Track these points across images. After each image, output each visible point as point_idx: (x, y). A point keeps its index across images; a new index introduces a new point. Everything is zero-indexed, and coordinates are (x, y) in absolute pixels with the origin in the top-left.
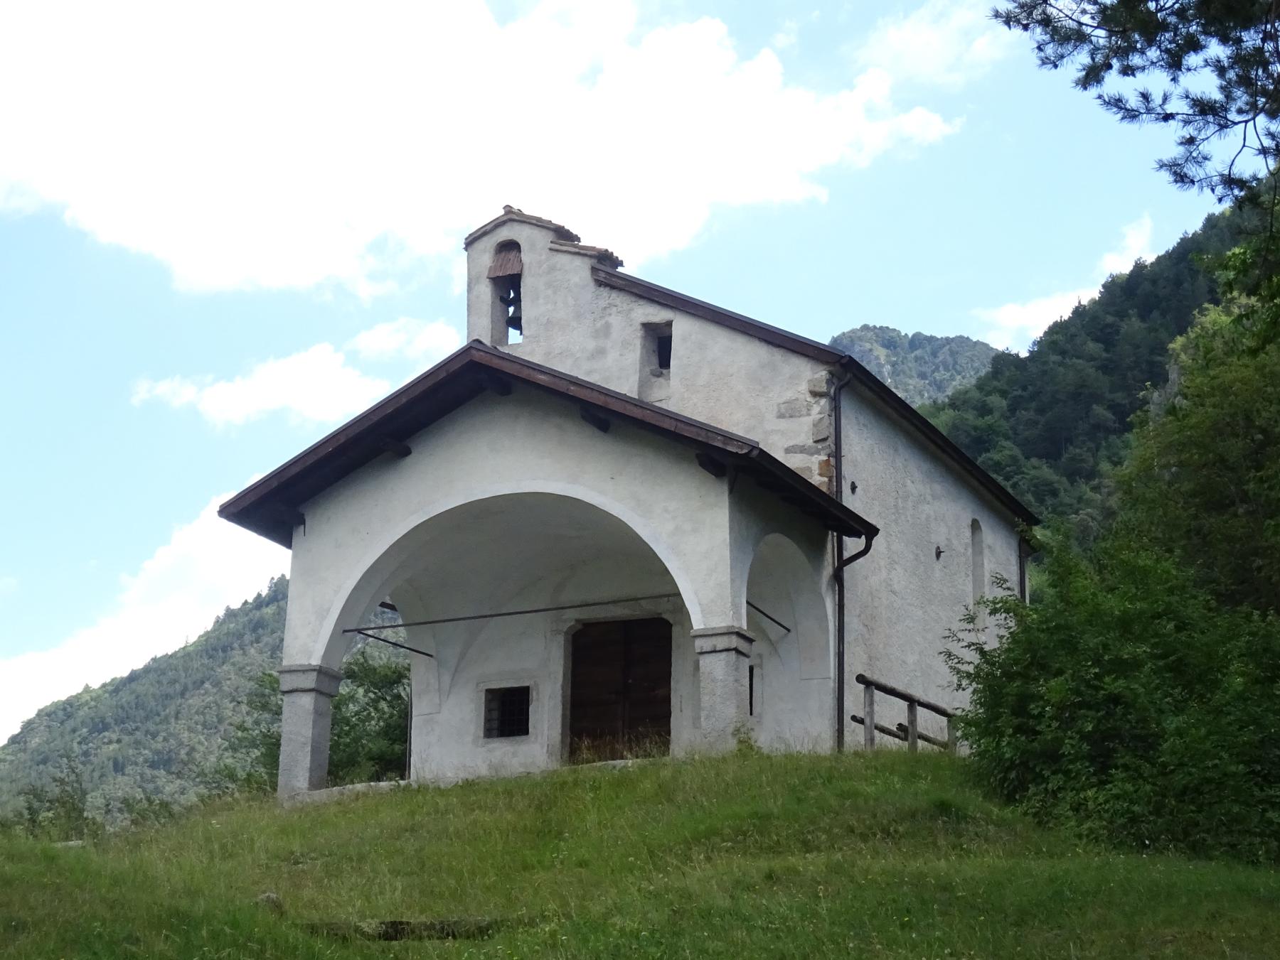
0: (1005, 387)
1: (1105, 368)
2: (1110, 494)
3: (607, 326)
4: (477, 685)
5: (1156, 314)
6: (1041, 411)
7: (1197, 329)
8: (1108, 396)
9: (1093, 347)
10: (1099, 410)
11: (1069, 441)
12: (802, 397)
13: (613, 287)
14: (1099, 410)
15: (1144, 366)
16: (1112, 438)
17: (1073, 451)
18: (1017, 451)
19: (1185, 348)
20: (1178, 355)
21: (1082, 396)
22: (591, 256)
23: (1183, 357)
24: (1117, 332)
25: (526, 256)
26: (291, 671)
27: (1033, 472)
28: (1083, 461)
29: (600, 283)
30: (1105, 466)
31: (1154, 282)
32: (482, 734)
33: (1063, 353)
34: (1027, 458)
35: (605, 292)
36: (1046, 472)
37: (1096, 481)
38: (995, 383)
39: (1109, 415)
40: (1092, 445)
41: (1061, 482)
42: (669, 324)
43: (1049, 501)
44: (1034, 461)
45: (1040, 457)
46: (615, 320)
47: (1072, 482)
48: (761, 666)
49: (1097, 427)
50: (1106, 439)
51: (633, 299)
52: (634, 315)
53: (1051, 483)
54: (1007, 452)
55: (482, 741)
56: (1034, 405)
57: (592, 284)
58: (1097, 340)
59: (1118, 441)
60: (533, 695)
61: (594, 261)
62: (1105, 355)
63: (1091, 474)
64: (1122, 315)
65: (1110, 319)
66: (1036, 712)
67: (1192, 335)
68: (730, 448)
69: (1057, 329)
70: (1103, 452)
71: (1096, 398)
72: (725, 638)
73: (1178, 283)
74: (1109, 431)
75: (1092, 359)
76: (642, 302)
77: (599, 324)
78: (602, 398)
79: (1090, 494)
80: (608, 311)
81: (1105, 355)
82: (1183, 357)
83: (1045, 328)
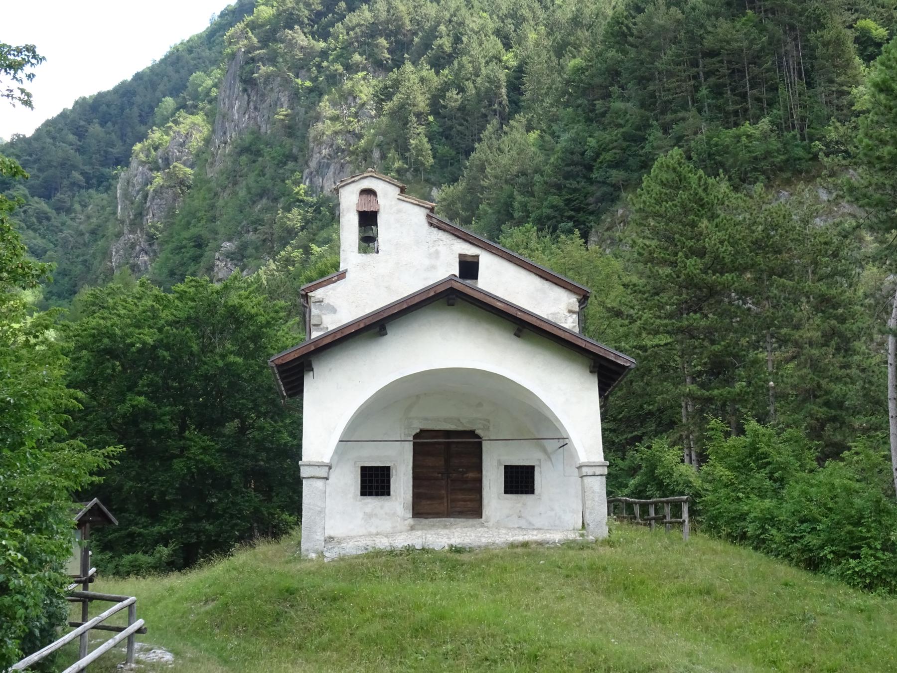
0: (20, 154)
1: (80, 150)
2: (80, 223)
3: (437, 253)
4: (355, 463)
5: (109, 124)
6: (40, 170)
7: (150, 141)
8: (81, 167)
9: (71, 138)
10: (76, 175)
11: (56, 189)
12: (561, 312)
13: (439, 228)
14: (76, 175)
15: (102, 152)
16: (83, 191)
17: (59, 195)
18: (26, 192)
19: (142, 150)
20: (138, 154)
21: (66, 166)
22: (427, 208)
23: (141, 155)
24: (87, 131)
25: (381, 200)
26: (309, 465)
27: (36, 205)
28: (65, 202)
29: (431, 225)
30: (77, 207)
31: (108, 106)
32: (359, 493)
33: (54, 138)
34: (33, 196)
35: (435, 231)
36: (43, 206)
37: (73, 215)
38: (12, 150)
39: (81, 178)
40: (69, 193)
41: (52, 213)
42: (477, 256)
43: (45, 223)
44: (36, 198)
45: (40, 197)
46: (442, 249)
47: (58, 213)
48: (540, 466)
49: (74, 184)
50: (79, 191)
51: (454, 238)
52: (454, 248)
53: (46, 213)
54: (21, 192)
55: (359, 497)
56: (36, 166)
57: (426, 225)
58: (74, 134)
59: (85, 194)
60: (393, 472)
61: (428, 211)
62: (79, 143)
63: (68, 211)
64: (89, 122)
65: (82, 123)
66: (84, 352)
67: (146, 144)
68: (619, 362)
69: (48, 123)
70: (76, 199)
71: (74, 167)
72: (601, 468)
73: (122, 109)
74: (80, 187)
75: (71, 144)
76: (459, 240)
77: (432, 250)
78: (538, 321)
79: (69, 222)
80: (437, 243)
81: (79, 143)
82: (141, 155)
83: (43, 121)
